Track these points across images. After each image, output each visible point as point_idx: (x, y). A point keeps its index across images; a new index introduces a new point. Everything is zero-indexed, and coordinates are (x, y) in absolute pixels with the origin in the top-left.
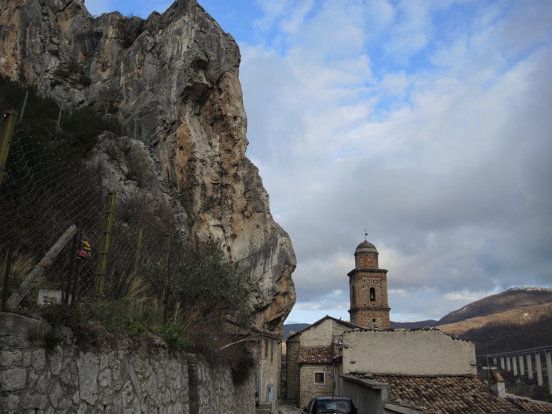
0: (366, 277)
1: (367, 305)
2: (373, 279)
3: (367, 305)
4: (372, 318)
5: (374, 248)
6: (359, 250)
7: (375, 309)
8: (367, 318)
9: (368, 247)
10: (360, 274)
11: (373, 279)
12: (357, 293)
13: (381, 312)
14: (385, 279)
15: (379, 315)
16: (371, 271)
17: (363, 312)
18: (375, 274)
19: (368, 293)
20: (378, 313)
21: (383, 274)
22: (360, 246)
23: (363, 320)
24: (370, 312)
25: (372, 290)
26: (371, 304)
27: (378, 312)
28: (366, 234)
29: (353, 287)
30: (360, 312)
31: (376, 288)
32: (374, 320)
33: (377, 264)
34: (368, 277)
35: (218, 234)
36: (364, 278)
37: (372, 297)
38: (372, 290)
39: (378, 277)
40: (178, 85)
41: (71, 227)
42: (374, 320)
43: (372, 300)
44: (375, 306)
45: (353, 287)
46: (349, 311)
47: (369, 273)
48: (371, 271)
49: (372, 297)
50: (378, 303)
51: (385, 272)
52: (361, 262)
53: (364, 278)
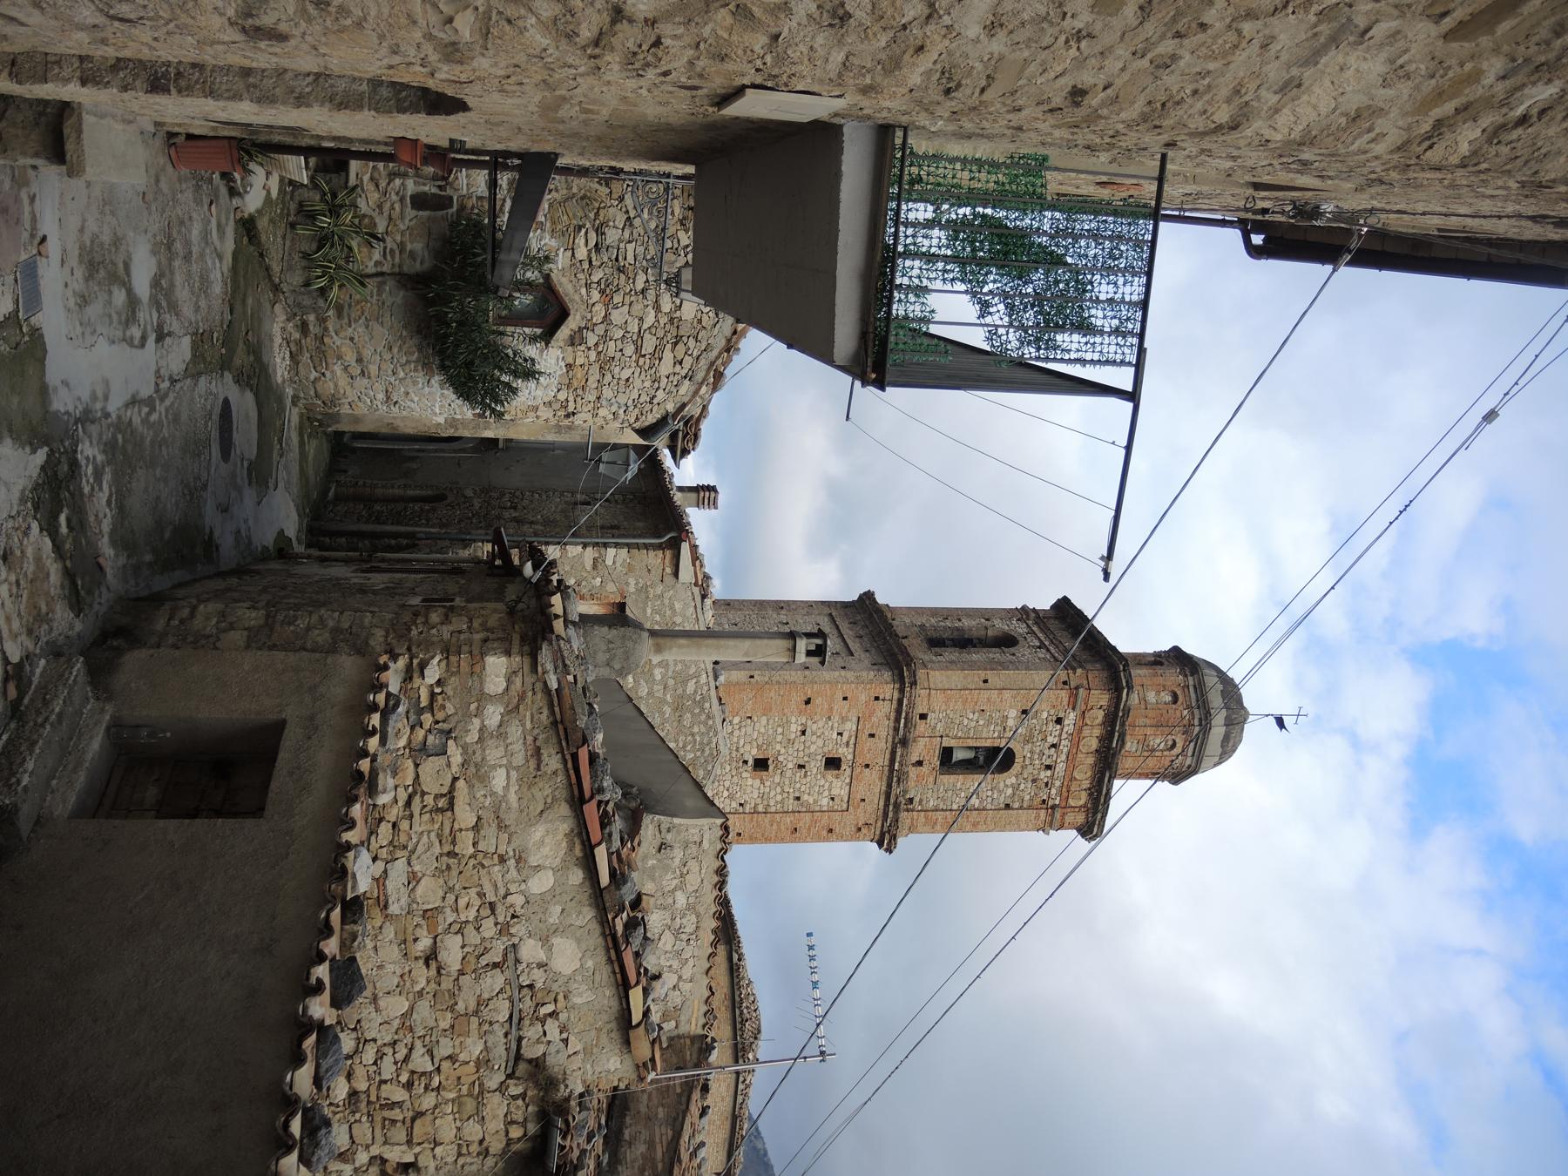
1: (921, 727)
2: (1060, 768)
3: (921, 727)
4: (845, 753)
6: (1211, 680)
7: (894, 775)
8: (850, 726)
9: (1226, 738)
10: (1100, 698)
11: (1060, 768)
12: (995, 678)
13: (875, 801)
14: (1051, 816)
15: (860, 790)
17: (885, 709)
20: (872, 785)
21: (1080, 818)
23: (839, 705)
25: (995, 759)
26: (924, 748)
27: (879, 786)
28: (1280, 722)
29: (1007, 641)
30: (889, 690)
31: (1009, 778)
32: (833, 763)
33: (1128, 776)
34: (1077, 738)
36: (1071, 719)
37: (959, 755)
38: (995, 759)
39: (1065, 792)
41: (363, 872)
42: (833, 763)
43: (947, 753)
44: (913, 772)
45: (1007, 641)
46: (868, 597)
47: (1094, 744)
49: (959, 755)
50: (926, 785)
51: (1091, 828)
52: (1151, 697)
53: (1071, 719)
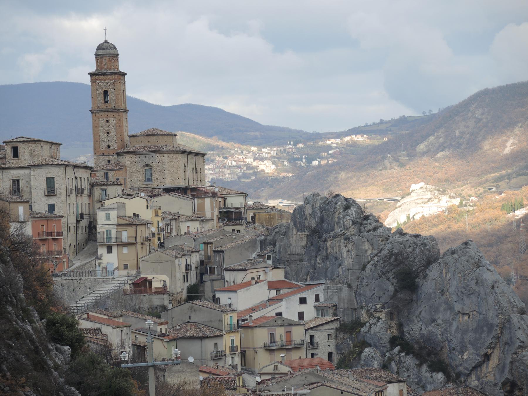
0: (100, 80)
1: (100, 107)
2: (107, 81)
3: (100, 107)
4: (105, 120)
5: (115, 48)
6: (101, 52)
7: (108, 111)
8: (101, 119)
11: (107, 81)
13: (114, 113)
16: (112, 74)
18: (108, 77)
19: (102, 95)
20: (110, 114)
22: (99, 48)
24: (103, 114)
25: (106, 93)
26: (104, 106)
27: (111, 113)
31: (110, 90)
32: (107, 121)
34: (101, 80)
35: (128, 163)
38: (106, 93)
39: (111, 79)
40: (382, 180)
42: (107, 121)
47: (102, 76)
48: (112, 74)
51: (124, 74)
53: (98, 81)
